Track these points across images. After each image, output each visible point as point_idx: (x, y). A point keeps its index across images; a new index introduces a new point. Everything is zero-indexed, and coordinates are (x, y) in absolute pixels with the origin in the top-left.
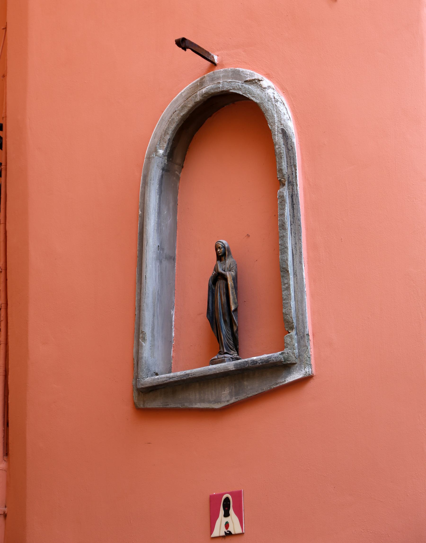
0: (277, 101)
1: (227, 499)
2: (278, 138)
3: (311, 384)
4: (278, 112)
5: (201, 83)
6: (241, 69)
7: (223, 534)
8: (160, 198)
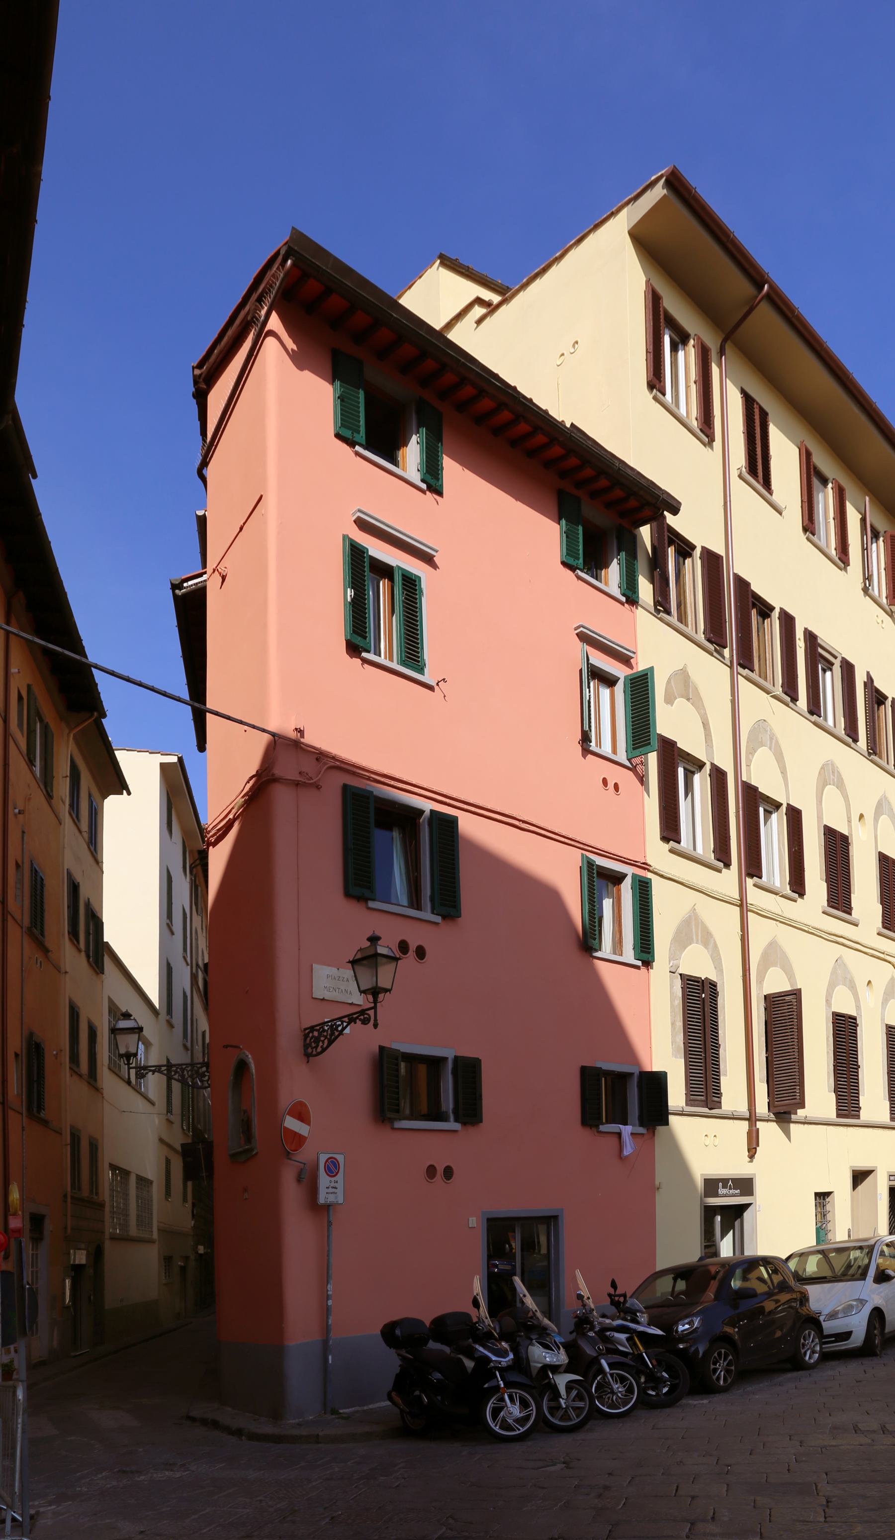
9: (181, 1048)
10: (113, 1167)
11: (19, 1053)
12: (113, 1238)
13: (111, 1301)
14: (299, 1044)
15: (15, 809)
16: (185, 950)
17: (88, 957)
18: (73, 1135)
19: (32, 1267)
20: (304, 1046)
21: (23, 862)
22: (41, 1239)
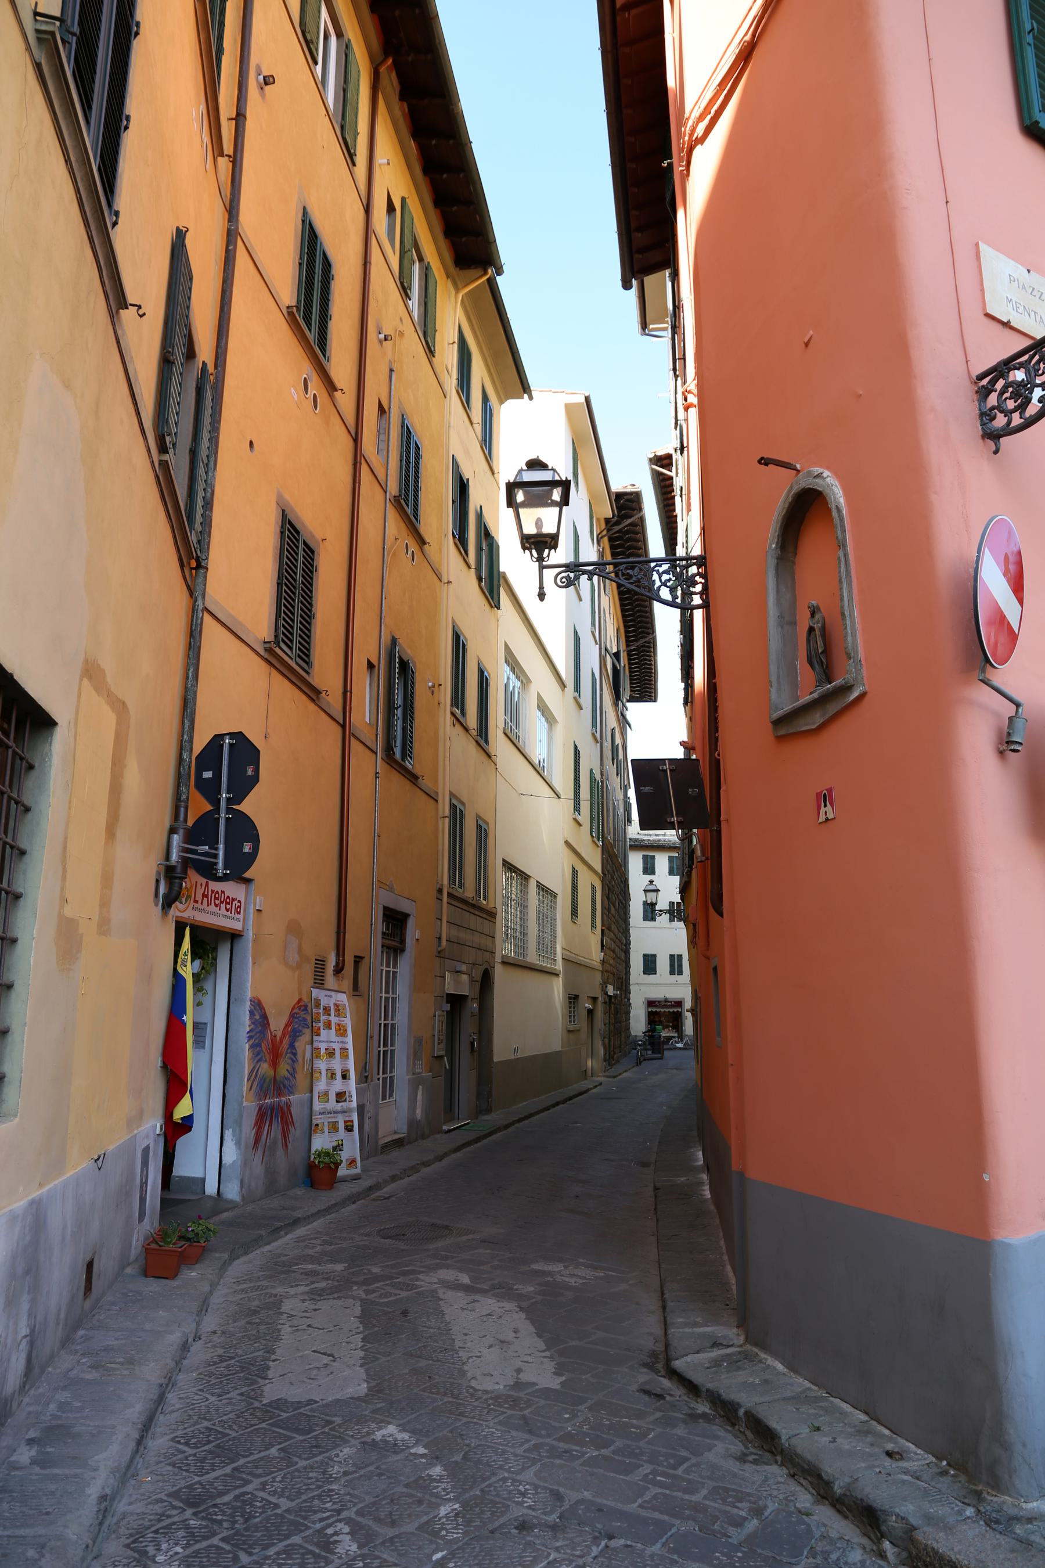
0: (832, 486)
1: (825, 794)
2: (835, 514)
3: (867, 698)
4: (834, 494)
5: (791, 487)
6: (811, 469)
7: (824, 820)
8: (777, 580)
9: (590, 737)
10: (508, 866)
11: (375, 662)
12: (506, 963)
13: (502, 1049)
14: (970, 409)
15: (380, 333)
16: (593, 624)
17: (480, 579)
18: (453, 807)
19: (387, 992)
20: (982, 414)
21: (390, 408)
22: (403, 950)
